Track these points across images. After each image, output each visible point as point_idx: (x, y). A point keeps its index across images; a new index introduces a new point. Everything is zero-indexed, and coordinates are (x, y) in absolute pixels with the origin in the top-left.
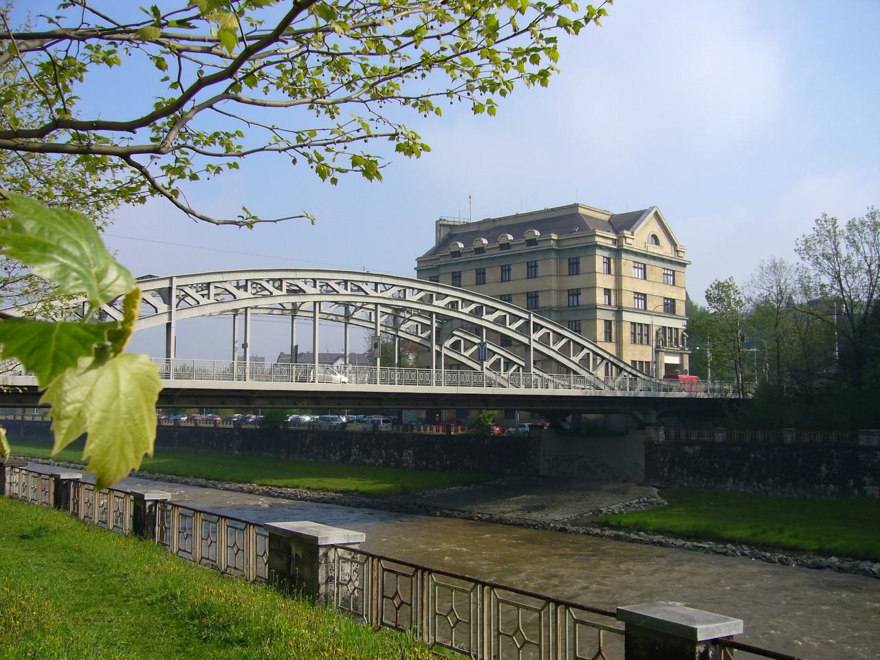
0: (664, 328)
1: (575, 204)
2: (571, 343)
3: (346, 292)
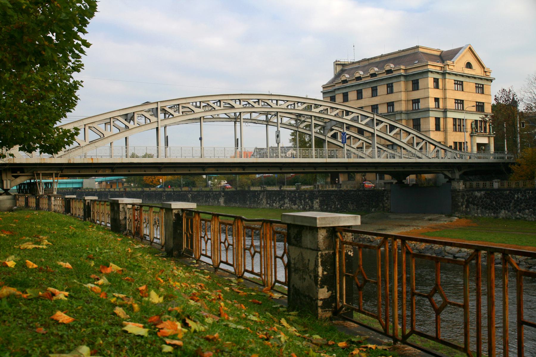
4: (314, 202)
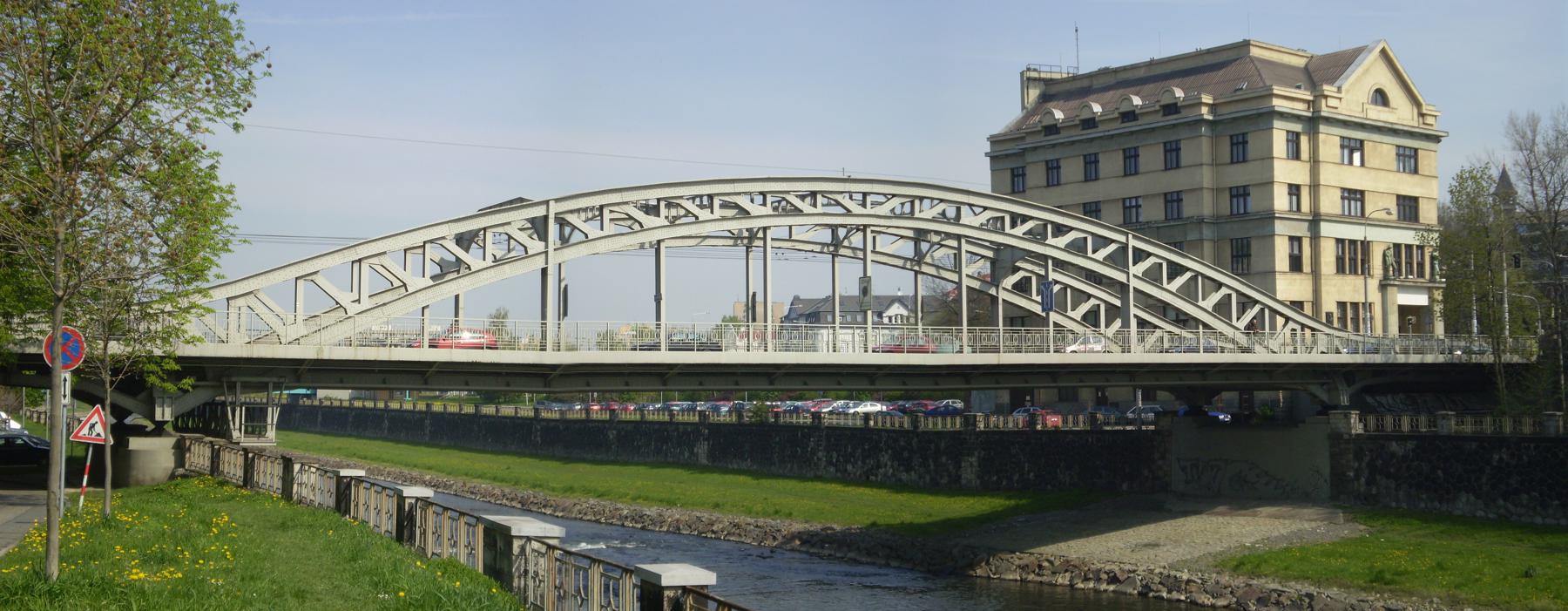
0: (1397, 246)
1: (1245, 41)
2: (1200, 278)
3: (813, 210)
4: (963, 464)
